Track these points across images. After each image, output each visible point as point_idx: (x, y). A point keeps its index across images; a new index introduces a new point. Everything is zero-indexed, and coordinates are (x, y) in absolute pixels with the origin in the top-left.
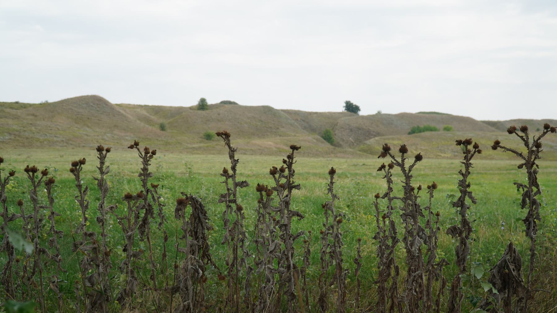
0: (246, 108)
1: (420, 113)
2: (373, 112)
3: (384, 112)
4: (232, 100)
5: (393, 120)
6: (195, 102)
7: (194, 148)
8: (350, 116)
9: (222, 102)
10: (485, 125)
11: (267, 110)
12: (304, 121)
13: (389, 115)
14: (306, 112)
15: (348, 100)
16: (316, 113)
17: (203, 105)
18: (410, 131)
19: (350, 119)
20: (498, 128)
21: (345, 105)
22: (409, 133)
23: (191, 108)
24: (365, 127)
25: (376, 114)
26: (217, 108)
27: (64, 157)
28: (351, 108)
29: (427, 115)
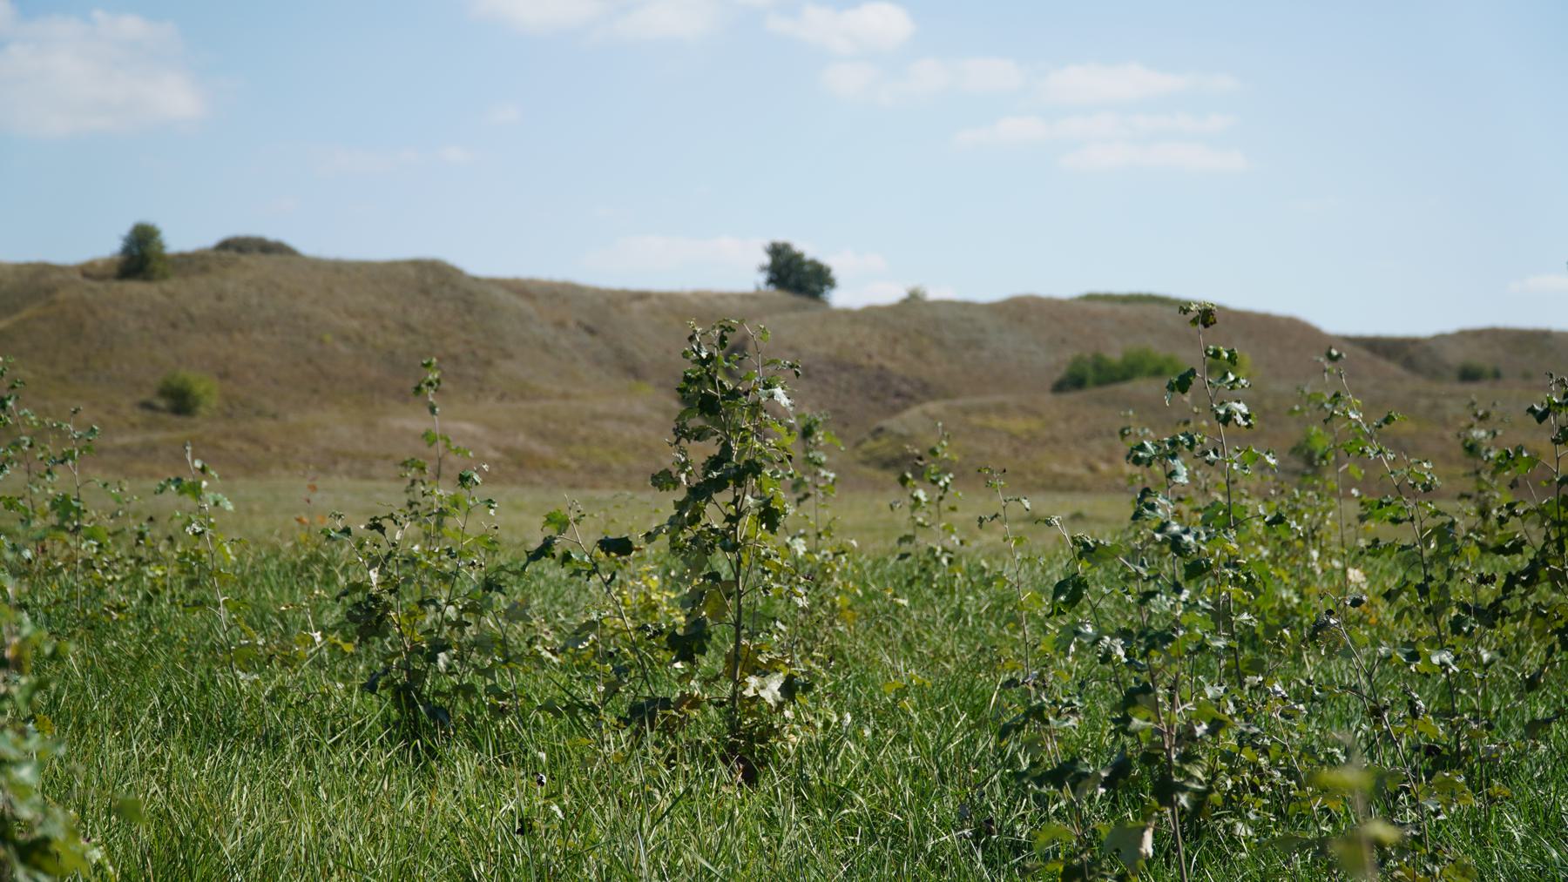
0: (338, 269)
1: (1091, 298)
2: (888, 293)
3: (934, 293)
4: (272, 234)
5: (982, 330)
6: (107, 245)
7: (126, 449)
8: (795, 308)
9: (225, 245)
10: (1365, 354)
11: (432, 280)
12: (591, 331)
13: (966, 306)
14: (598, 292)
15: (781, 238)
16: (642, 296)
17: (141, 256)
18: (1057, 376)
19: (789, 324)
20: (1410, 364)
21: (766, 260)
22: (1059, 388)
23: (88, 272)
24: (864, 361)
25: (905, 302)
26: (205, 270)
27: (1493, 413)
28: (795, 275)
29: (1124, 309)
